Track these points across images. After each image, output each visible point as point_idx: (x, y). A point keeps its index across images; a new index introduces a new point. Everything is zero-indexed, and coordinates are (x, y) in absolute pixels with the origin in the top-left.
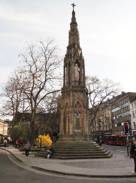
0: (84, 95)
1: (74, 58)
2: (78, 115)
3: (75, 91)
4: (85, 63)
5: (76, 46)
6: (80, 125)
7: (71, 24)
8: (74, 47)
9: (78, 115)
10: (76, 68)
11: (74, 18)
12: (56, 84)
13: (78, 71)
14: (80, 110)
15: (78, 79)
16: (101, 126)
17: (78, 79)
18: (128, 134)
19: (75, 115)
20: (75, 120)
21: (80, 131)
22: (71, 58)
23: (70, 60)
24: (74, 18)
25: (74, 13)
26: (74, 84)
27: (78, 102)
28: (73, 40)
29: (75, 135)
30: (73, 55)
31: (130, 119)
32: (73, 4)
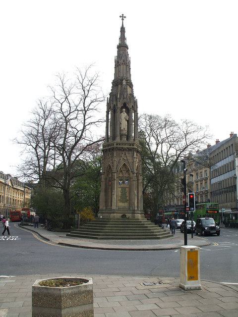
0: (133, 155)
1: (122, 100)
2: (123, 183)
4: (138, 104)
5: (124, 82)
7: (118, 47)
8: (122, 84)
10: (124, 115)
11: (123, 38)
12: (97, 132)
17: (125, 132)
20: (120, 189)
22: (116, 100)
24: (123, 38)
25: (123, 30)
32: (123, 15)
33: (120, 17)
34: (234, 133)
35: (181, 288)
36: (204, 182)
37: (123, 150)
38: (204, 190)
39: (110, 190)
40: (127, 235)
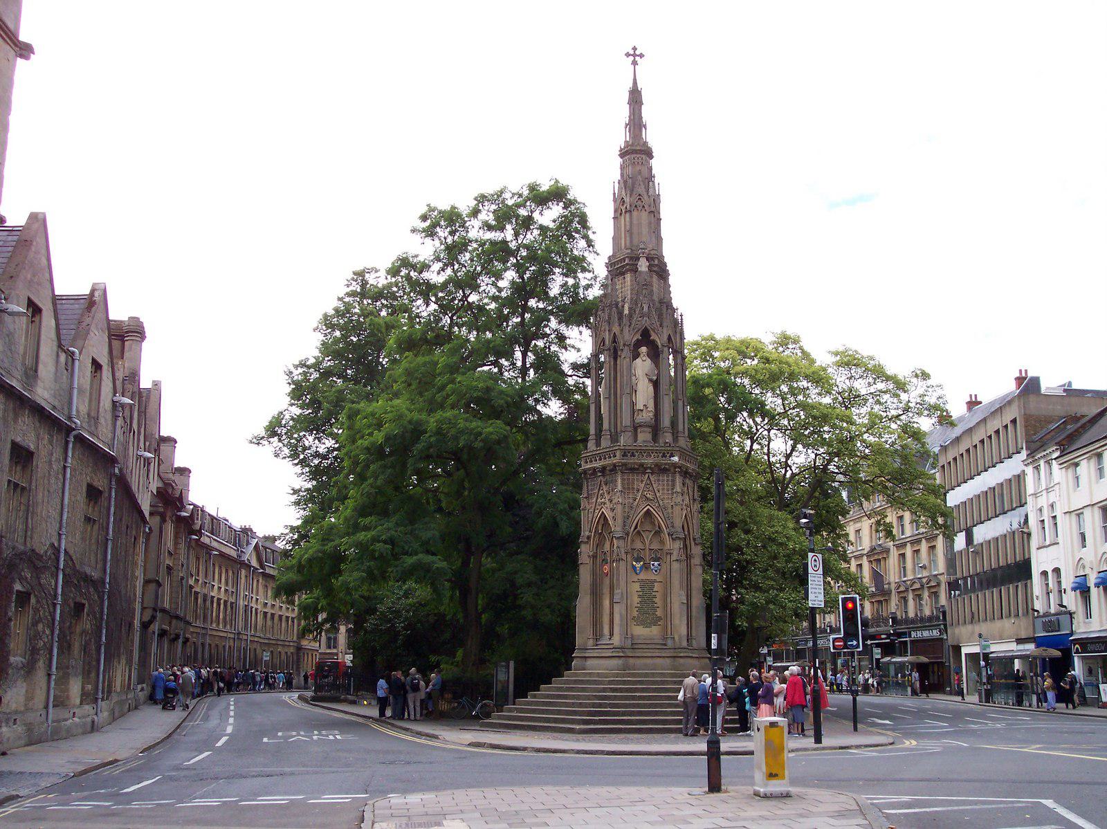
0: (673, 485)
3: (632, 470)
5: (643, 265)
6: (655, 609)
8: (634, 270)
9: (646, 567)
10: (643, 366)
11: (636, 124)
13: (650, 380)
14: (655, 546)
15: (651, 414)
16: (889, 593)
17: (647, 416)
18: (855, 643)
19: (634, 567)
20: (637, 587)
21: (654, 631)
23: (616, 329)
24: (636, 124)
25: (635, 98)
26: (630, 441)
27: (648, 513)
28: (631, 235)
29: (632, 648)
30: (626, 312)
31: (1029, 554)
32: (635, 49)
33: (628, 55)
34: (1030, 375)
35: (757, 794)
36: (924, 546)
37: (641, 469)
38: (925, 573)
39: (606, 590)
40: (656, 722)
